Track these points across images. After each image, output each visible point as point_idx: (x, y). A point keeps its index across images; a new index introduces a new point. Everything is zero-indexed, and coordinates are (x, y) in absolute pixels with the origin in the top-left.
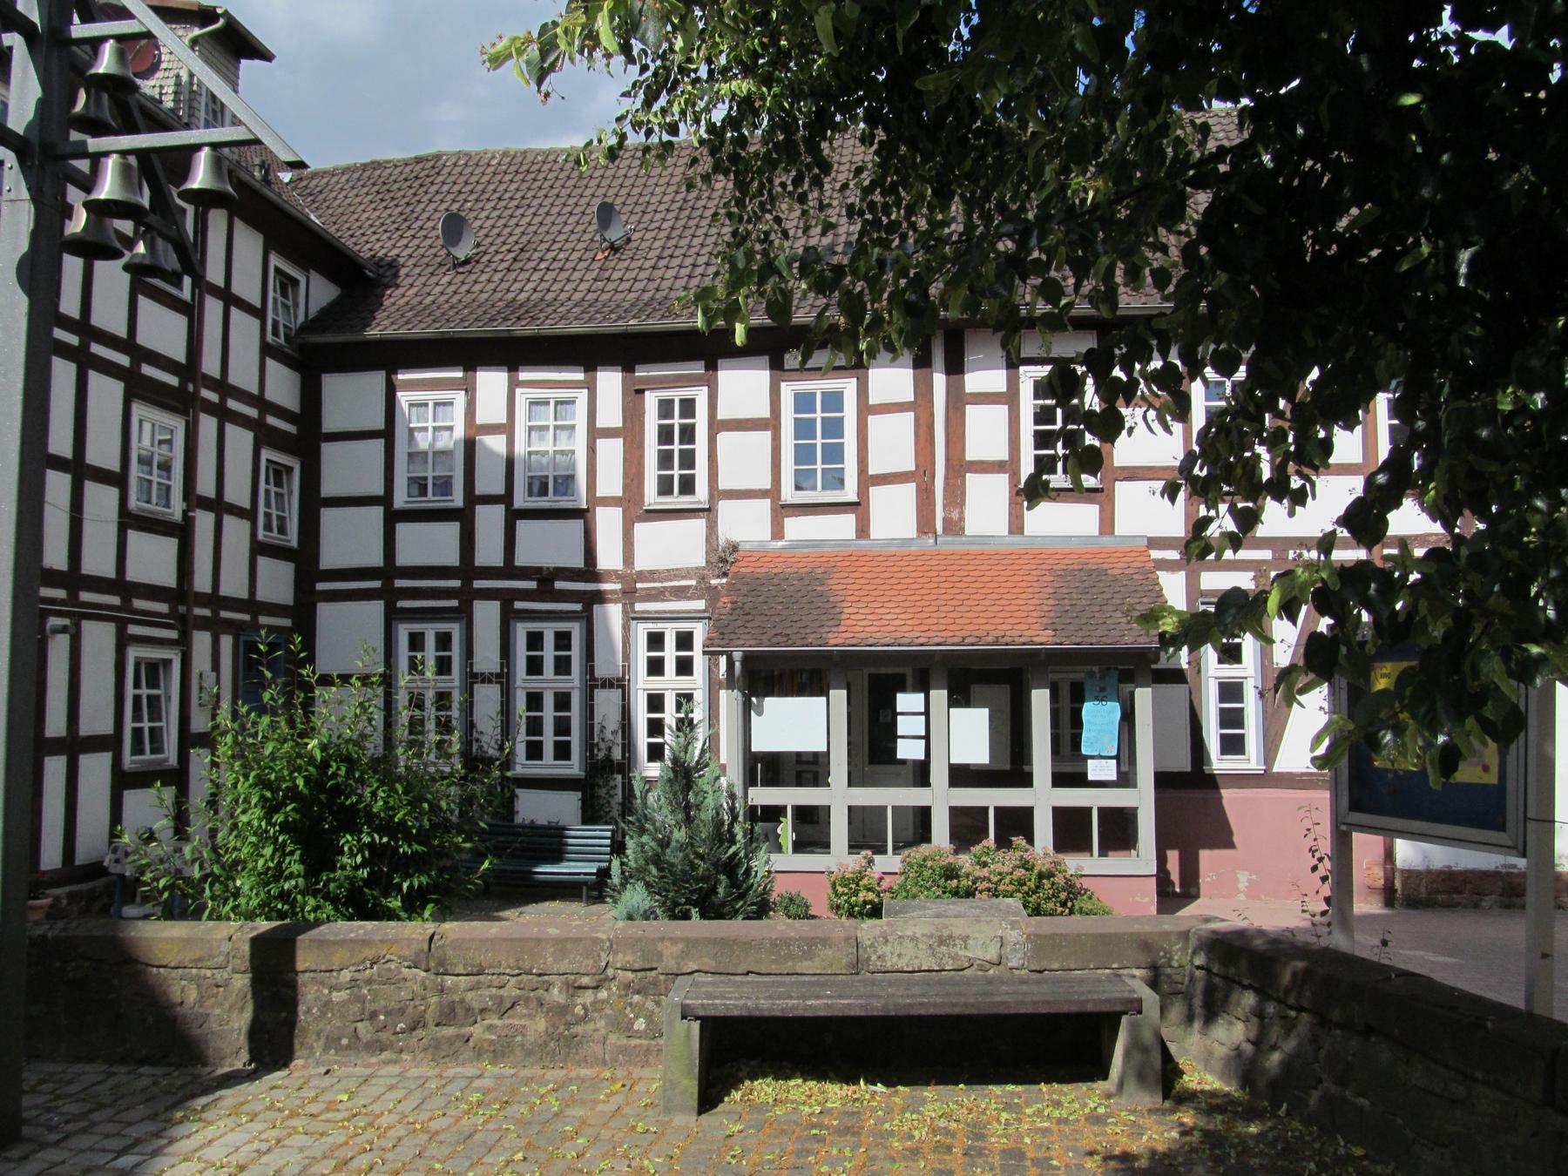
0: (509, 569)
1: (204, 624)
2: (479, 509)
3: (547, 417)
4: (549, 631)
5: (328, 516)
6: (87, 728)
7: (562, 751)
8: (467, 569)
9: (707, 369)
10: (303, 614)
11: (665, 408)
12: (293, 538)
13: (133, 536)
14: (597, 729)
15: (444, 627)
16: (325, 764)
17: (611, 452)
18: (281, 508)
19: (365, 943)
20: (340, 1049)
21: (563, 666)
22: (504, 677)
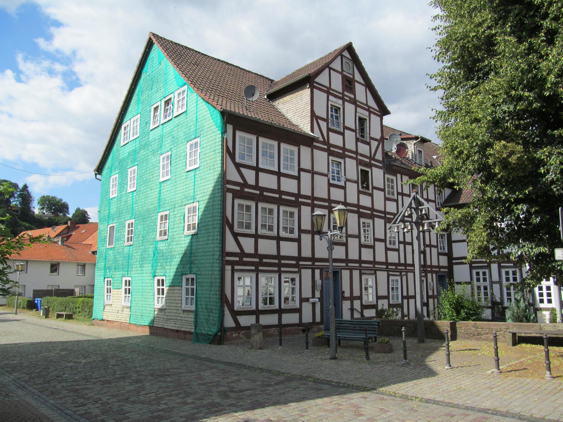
1: (430, 272)
4: (511, 271)
5: (454, 245)
12: (446, 251)
15: (484, 270)
16: (458, 299)
18: (443, 244)
21: (485, 280)
22: (500, 282)
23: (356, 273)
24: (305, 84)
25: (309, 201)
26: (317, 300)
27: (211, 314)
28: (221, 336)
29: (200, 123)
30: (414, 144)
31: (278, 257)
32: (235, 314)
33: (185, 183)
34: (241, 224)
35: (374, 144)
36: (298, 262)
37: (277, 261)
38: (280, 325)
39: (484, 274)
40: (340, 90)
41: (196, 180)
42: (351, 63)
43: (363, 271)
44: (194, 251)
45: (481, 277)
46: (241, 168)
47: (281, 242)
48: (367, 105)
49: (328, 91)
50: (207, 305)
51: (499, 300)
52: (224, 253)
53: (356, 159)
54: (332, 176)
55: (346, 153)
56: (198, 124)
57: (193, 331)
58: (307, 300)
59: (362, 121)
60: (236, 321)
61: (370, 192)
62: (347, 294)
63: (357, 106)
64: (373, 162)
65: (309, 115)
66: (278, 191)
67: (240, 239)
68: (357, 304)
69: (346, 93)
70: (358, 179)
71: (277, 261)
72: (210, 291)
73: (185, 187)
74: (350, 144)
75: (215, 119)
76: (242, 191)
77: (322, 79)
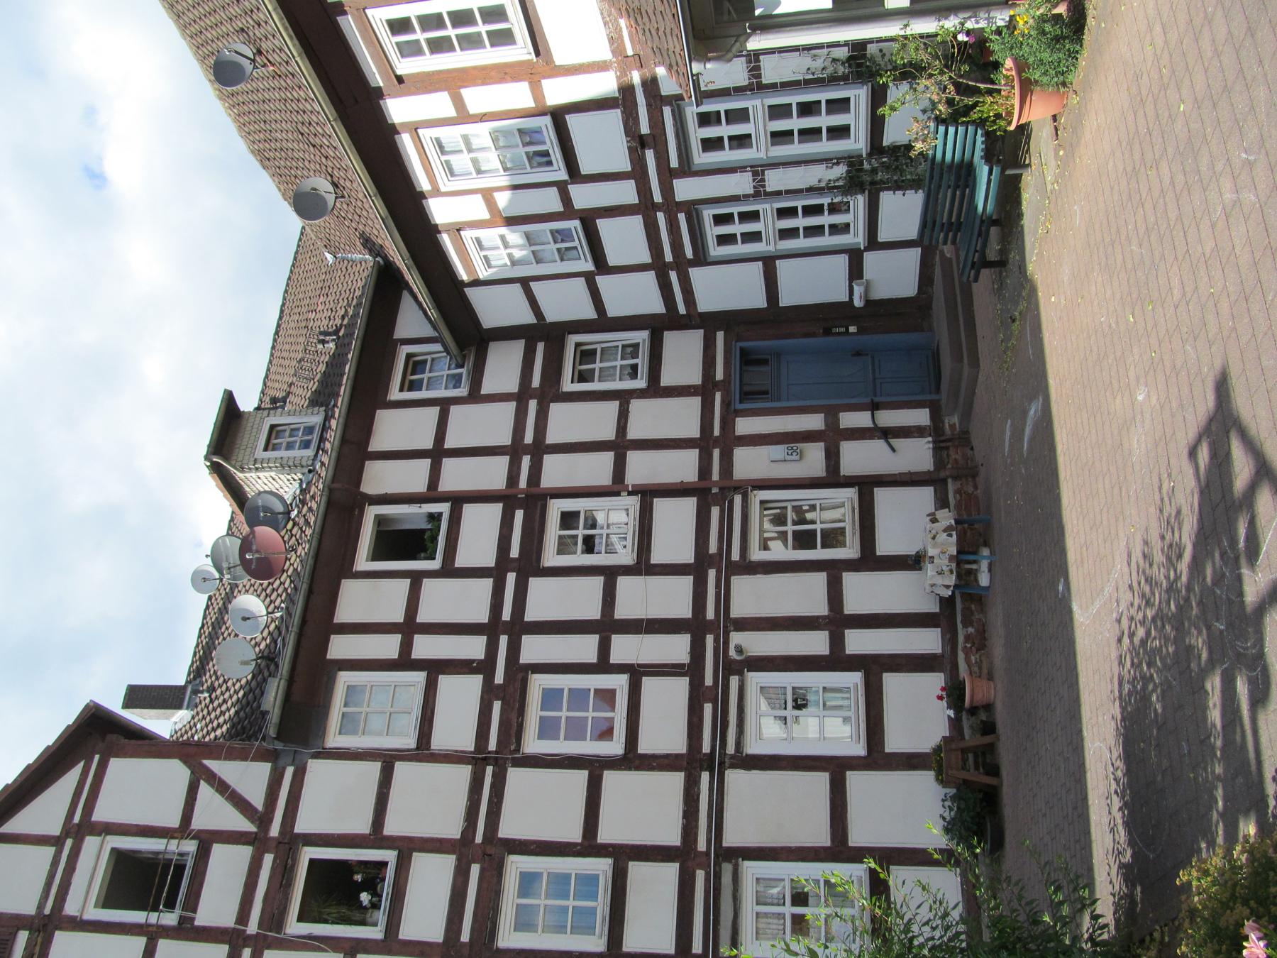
3: (461, 162)
6: (820, 607)
7: (840, 105)
9: (345, 13)
10: (710, 323)
11: (411, 50)
12: (641, 337)
17: (478, 98)
22: (758, 170)
30: (242, 469)
51: (841, 170)
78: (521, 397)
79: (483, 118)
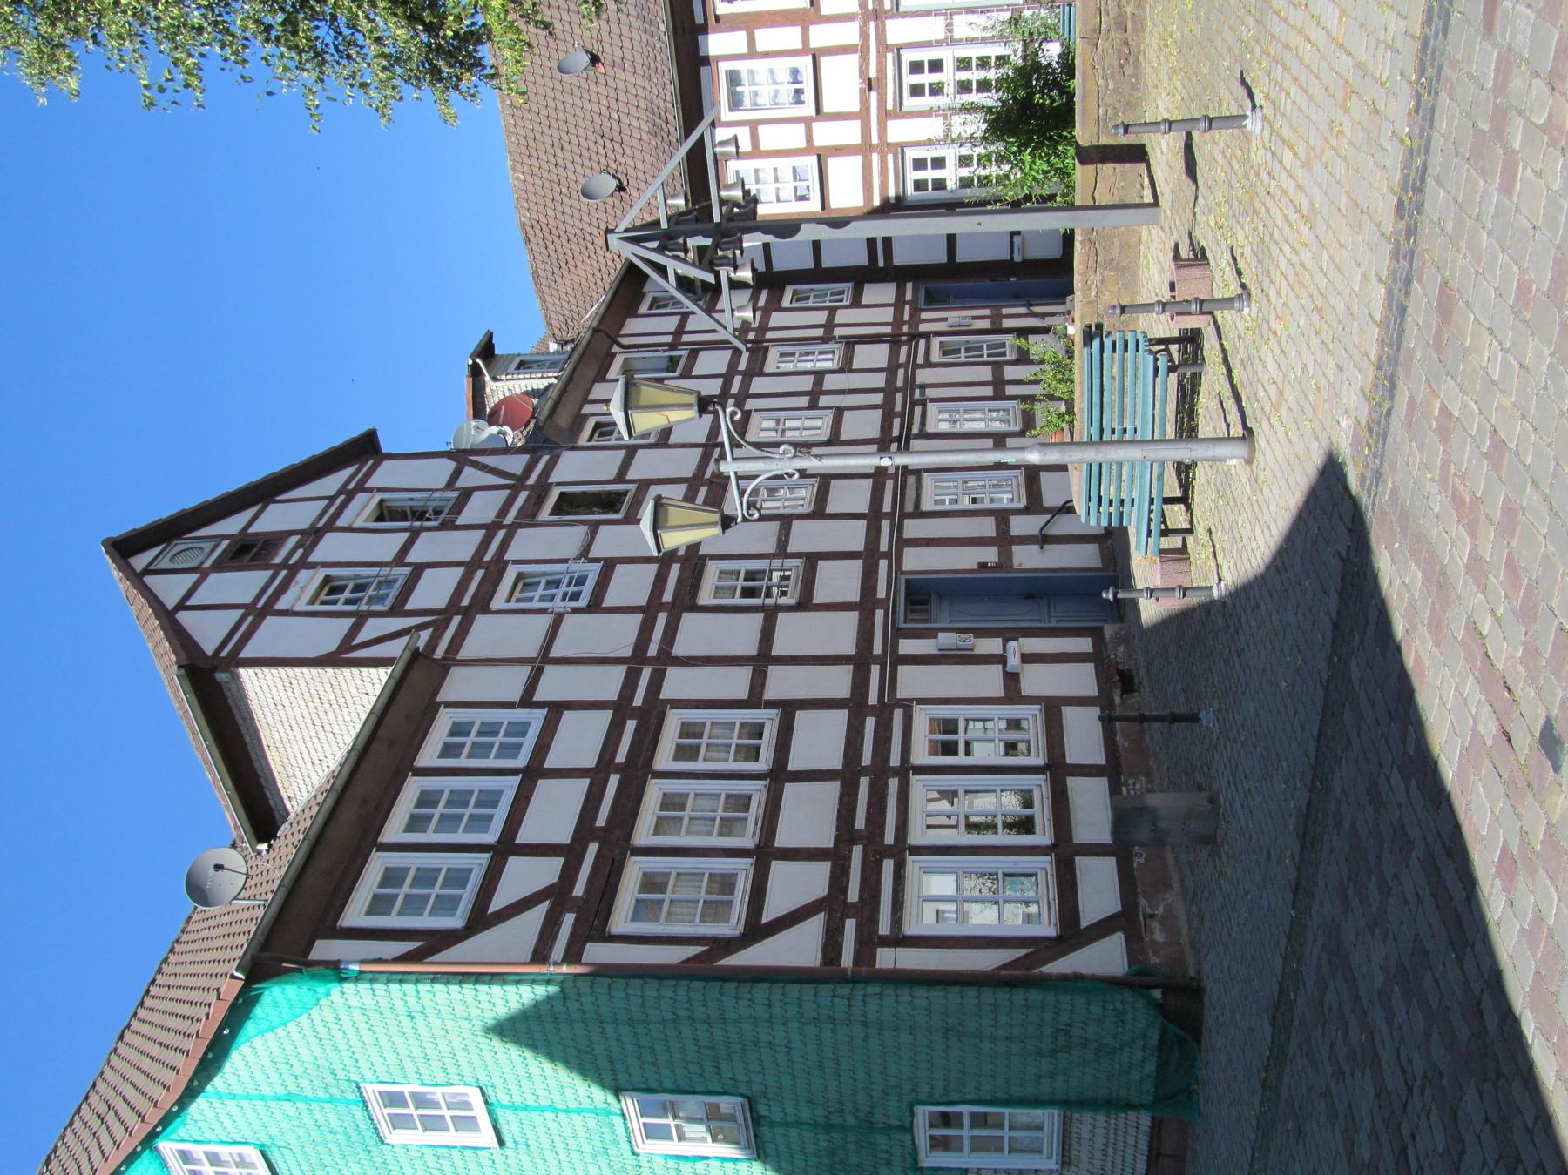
0: (863, 115)
2: (816, 144)
8: (864, 149)
12: (847, 286)
13: (830, 509)
14: (985, 34)
19: (1084, 73)
20: (1138, 82)
23: (913, 528)
24: (219, 687)
25: (647, 672)
26: (1012, 644)
27: (1076, 1031)
28: (1166, 989)
29: (304, 1082)
30: (495, 379)
31: (847, 776)
32: (1072, 934)
33: (549, 1154)
34: (715, 910)
35: (470, 477)
36: (871, 708)
37: (864, 782)
38: (1112, 770)
39: (916, 67)
40: (265, 575)
41: (531, 1101)
42: (179, 546)
43: (909, 508)
44: (819, 1111)
45: (926, 78)
46: (491, 910)
47: (776, 651)
48: (332, 499)
49: (258, 611)
50: (1039, 1053)
52: (827, 974)
53: (512, 530)
54: (563, 600)
55: (488, 557)
56: (309, 1093)
57: (1145, 1119)
58: (1012, 679)
59: (385, 513)
60: (1102, 929)
61: (632, 487)
62: (990, 555)
63: (330, 527)
64: (532, 480)
65: (330, 671)
66: (597, 776)
67: (770, 913)
68: (1022, 526)
69: (278, 560)
70: (583, 522)
71: (864, 782)
72: (979, 1036)
73: (562, 1156)
74: (462, 545)
75: (286, 1011)
76: (581, 907)
77: (209, 631)
78: (649, 611)
79: (767, 55)
